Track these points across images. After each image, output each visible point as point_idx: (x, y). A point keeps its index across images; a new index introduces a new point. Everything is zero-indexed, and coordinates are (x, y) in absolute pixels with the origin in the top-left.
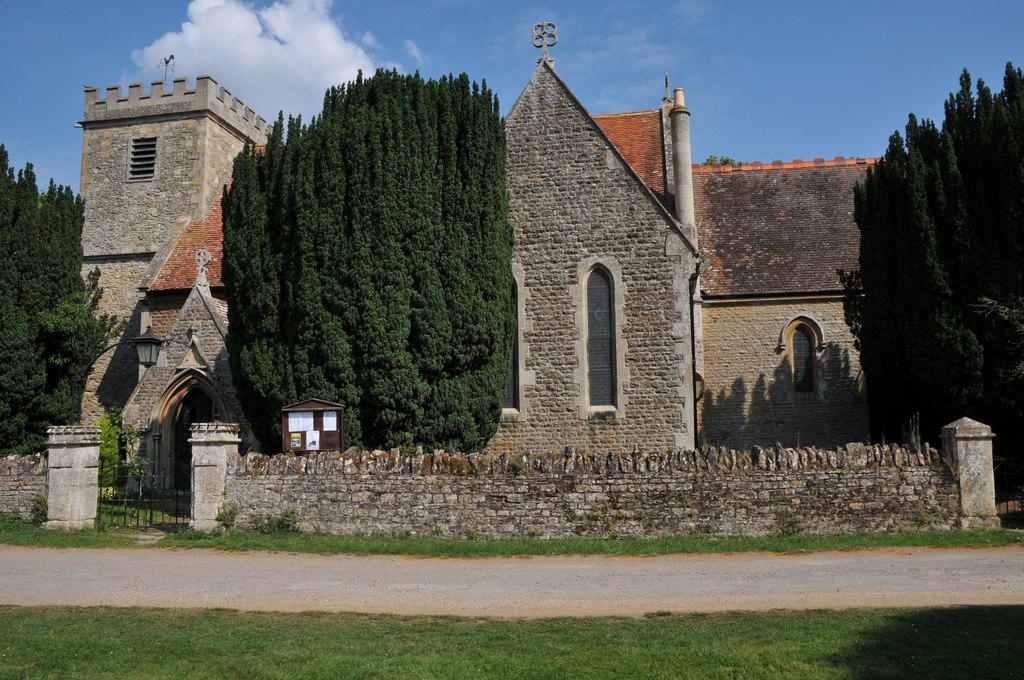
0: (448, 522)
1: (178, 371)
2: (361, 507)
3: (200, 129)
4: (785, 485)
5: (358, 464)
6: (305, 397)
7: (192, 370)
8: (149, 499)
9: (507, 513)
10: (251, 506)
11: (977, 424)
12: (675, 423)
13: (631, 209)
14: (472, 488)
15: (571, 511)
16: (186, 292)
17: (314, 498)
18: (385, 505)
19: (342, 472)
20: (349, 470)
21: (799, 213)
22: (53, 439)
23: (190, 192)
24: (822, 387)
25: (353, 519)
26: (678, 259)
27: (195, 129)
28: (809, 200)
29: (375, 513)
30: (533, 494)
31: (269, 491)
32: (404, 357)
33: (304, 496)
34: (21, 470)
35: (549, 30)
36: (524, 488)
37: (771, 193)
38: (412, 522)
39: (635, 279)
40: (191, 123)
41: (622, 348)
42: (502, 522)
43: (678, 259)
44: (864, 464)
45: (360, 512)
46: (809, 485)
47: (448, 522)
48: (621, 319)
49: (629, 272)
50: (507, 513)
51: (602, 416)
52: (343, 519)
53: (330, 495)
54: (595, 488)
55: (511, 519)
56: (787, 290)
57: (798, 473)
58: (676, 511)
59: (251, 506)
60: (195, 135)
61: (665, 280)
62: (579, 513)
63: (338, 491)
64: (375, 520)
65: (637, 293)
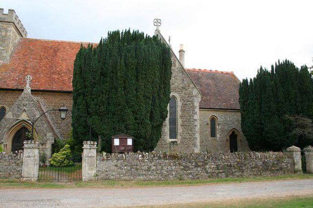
0: (173, 175)
1: (17, 120)
2: (145, 171)
3: (9, 29)
4: (258, 163)
5: (143, 156)
6: (123, 133)
7: (24, 120)
8: (59, 167)
9: (189, 171)
10: (106, 171)
11: (297, 148)
12: (195, 145)
13: (183, 80)
14: (179, 164)
15: (207, 171)
16: (22, 90)
17: (129, 168)
18: (153, 170)
19: (138, 159)
20: (140, 159)
21: (208, 85)
22: (26, 146)
23: (3, 52)
24: (218, 136)
25: (143, 175)
26: (196, 96)
27: (6, 29)
28: (210, 81)
29: (150, 173)
30: (197, 166)
31: (111, 164)
32: (148, 122)
33: (126, 167)
34: (10, 158)
35: (159, 21)
36: (194, 164)
37: (199, 78)
38: (162, 175)
39: (184, 101)
40: (5, 26)
41: (180, 121)
42: (188, 175)
43: (196, 96)
44: (46, 164)
45: (144, 173)
46: (263, 163)
47: (173, 175)
48: (179, 113)
49: (182, 99)
50: (189, 171)
51: (173, 142)
52: (139, 175)
53: (134, 167)
54: (213, 164)
55: (191, 173)
56: (210, 107)
57: (261, 159)
58: (233, 170)
59: (106, 171)
60: (7, 31)
61: (192, 102)
62: (209, 171)
63: (137, 165)
64: (150, 175)
65: (184, 105)
